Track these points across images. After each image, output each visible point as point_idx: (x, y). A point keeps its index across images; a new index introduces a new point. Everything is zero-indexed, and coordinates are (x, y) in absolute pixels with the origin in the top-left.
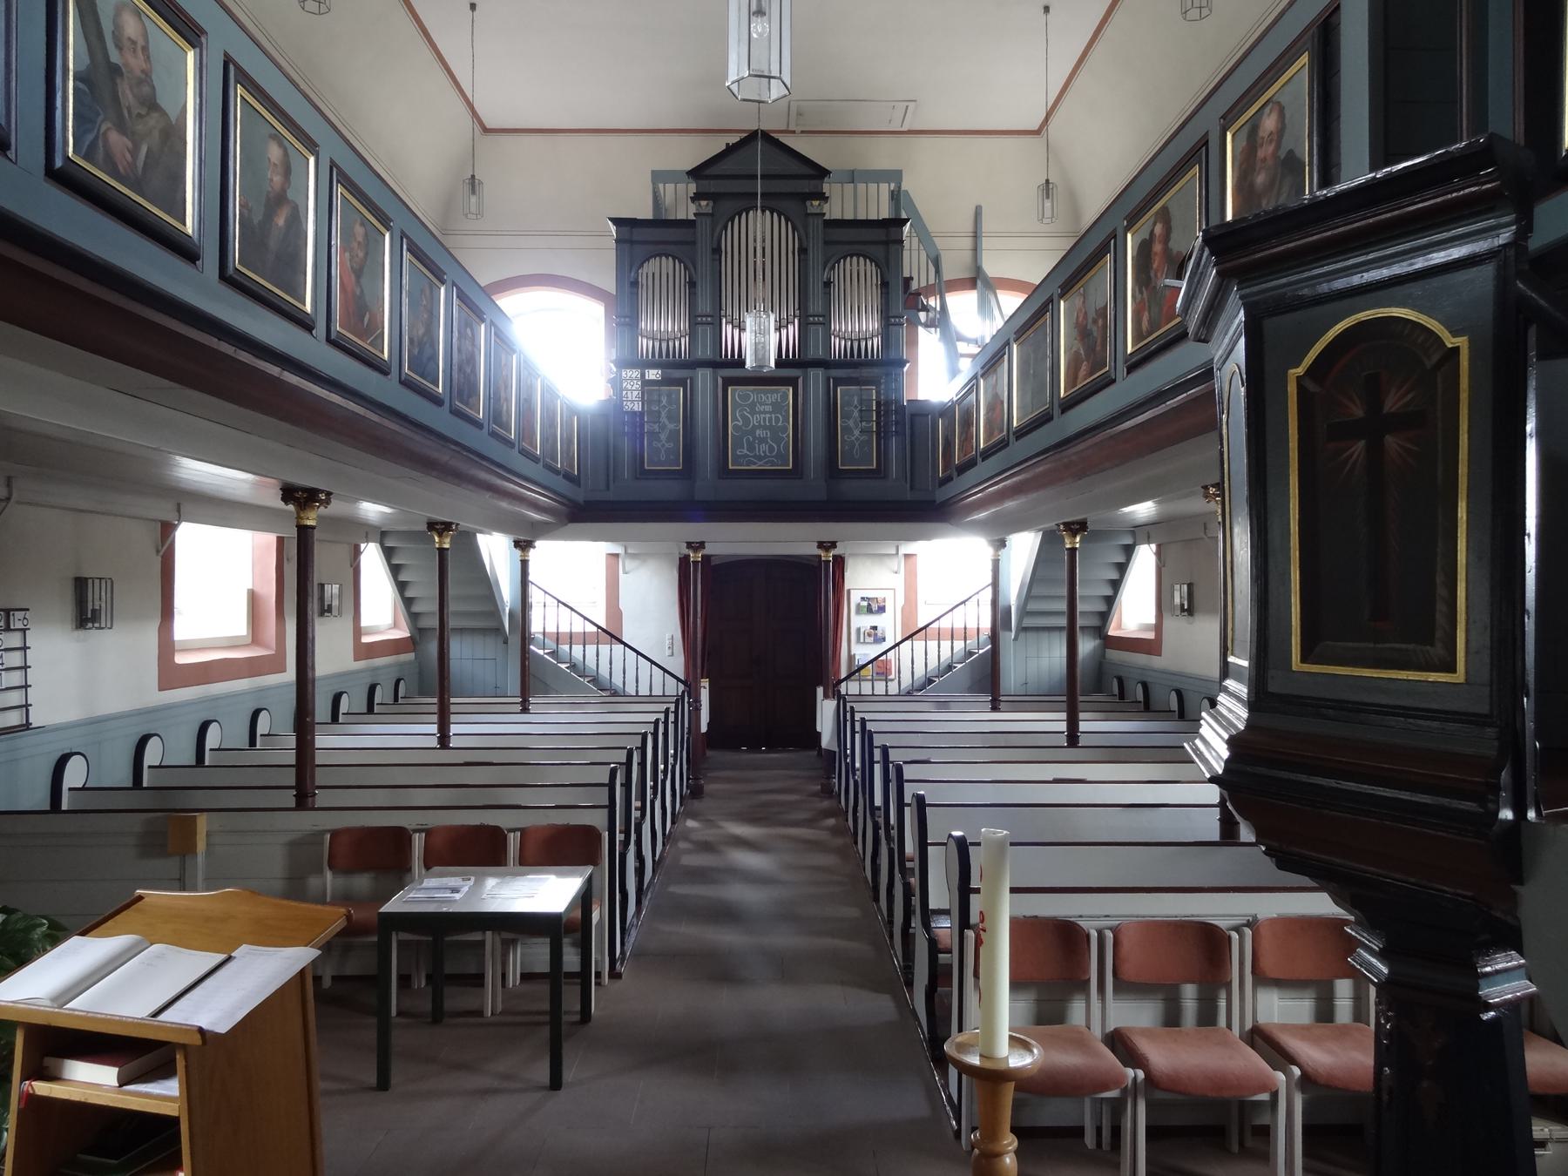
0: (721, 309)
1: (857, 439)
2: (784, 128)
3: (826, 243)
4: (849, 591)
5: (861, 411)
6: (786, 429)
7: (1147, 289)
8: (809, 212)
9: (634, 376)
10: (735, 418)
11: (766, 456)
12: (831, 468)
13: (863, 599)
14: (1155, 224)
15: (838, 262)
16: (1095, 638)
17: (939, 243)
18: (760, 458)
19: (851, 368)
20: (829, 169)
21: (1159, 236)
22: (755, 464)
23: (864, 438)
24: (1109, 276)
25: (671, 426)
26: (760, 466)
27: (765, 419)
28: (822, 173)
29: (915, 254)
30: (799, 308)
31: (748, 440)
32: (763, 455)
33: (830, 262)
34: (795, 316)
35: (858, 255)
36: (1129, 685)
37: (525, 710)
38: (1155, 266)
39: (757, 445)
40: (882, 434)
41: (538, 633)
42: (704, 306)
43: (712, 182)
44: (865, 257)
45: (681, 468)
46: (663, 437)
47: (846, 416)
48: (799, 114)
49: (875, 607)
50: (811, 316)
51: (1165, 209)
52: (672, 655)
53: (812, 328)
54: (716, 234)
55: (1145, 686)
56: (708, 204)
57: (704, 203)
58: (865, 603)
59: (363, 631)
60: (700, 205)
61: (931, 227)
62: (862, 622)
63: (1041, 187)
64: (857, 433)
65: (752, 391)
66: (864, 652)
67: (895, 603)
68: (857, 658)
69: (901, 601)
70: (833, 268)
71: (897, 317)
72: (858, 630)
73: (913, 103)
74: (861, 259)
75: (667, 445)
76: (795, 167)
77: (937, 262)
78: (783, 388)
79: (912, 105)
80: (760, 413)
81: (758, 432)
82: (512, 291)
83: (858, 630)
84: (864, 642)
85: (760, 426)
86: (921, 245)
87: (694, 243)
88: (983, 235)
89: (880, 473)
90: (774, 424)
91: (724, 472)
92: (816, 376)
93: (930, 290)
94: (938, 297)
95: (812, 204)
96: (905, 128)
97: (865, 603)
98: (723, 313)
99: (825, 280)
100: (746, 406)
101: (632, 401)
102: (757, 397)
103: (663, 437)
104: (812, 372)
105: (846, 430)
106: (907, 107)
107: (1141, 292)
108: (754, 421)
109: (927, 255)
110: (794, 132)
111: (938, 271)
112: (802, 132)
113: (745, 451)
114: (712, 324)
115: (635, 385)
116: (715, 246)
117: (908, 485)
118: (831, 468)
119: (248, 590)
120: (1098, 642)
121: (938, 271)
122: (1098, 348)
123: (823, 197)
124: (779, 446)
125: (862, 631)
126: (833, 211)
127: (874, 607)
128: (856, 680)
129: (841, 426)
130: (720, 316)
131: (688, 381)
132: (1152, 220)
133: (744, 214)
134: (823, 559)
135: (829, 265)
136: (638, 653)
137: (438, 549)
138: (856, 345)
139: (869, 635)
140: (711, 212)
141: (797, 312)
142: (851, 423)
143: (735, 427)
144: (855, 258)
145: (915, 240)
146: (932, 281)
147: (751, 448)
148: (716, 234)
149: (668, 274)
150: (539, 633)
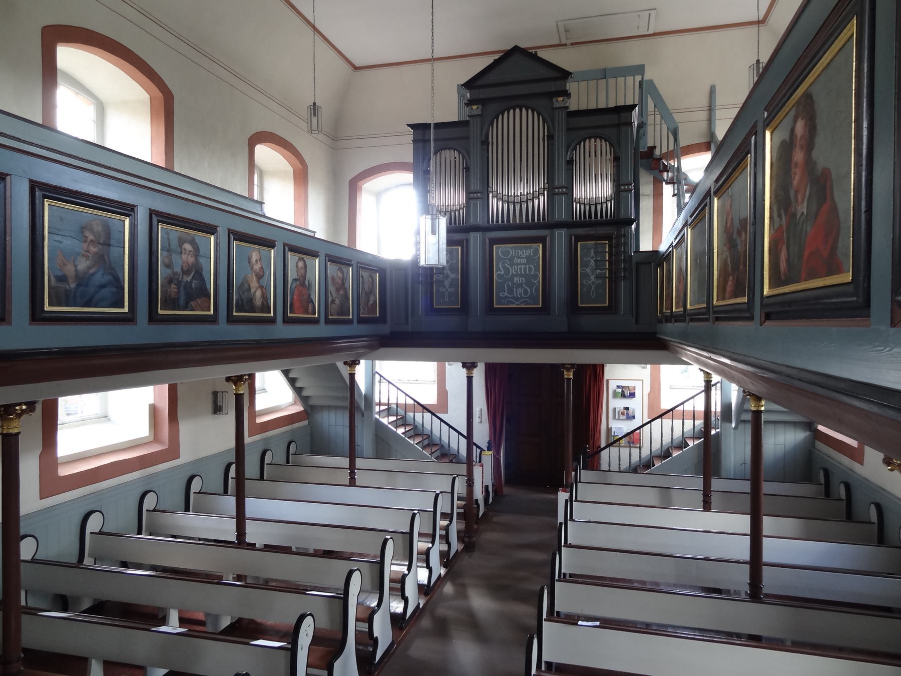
0: (488, 186)
1: (593, 283)
2: (557, 42)
3: (569, 129)
4: (608, 381)
5: (596, 261)
6: (536, 276)
7: (786, 214)
8: (555, 106)
10: (498, 269)
11: (522, 297)
12: (572, 306)
13: (618, 387)
14: (795, 121)
15: (579, 144)
16: (805, 430)
17: (677, 117)
18: (517, 299)
19: (589, 227)
20: (571, 71)
21: (801, 138)
22: (513, 303)
23: (599, 281)
24: (749, 181)
25: (452, 276)
26: (518, 305)
27: (521, 269)
28: (565, 75)
29: (658, 127)
30: (548, 183)
31: (509, 284)
32: (519, 296)
33: (572, 146)
34: (544, 189)
35: (595, 137)
36: (835, 480)
37: (352, 483)
38: (795, 182)
39: (515, 289)
40: (614, 279)
41: (393, 404)
42: (476, 185)
43: (481, 90)
44: (601, 138)
45: (459, 307)
46: (447, 283)
47: (585, 265)
48: (566, 31)
49: (627, 393)
50: (557, 188)
51: (808, 96)
52: (481, 422)
53: (557, 197)
54: (484, 130)
55: (848, 487)
56: (478, 108)
57: (475, 107)
58: (620, 390)
59: (257, 414)
60: (472, 109)
61: (670, 105)
62: (619, 404)
63: (752, 67)
64: (592, 278)
65: (512, 248)
66: (621, 427)
67: (643, 391)
68: (613, 430)
69: (647, 390)
70: (575, 149)
71: (626, 185)
72: (615, 409)
73: (655, 11)
74: (598, 140)
75: (449, 290)
76: (544, 72)
77: (675, 133)
78: (535, 245)
79: (653, 13)
80: (517, 264)
81: (515, 279)
82: (375, 176)
83: (615, 409)
84: (619, 419)
85: (517, 275)
86: (663, 121)
87: (467, 138)
88: (717, 108)
89: (612, 308)
90: (528, 272)
91: (490, 308)
92: (561, 235)
93: (670, 155)
94: (676, 160)
95: (557, 101)
96: (651, 32)
97: (620, 390)
98: (490, 189)
99: (568, 159)
100: (507, 259)
102: (515, 252)
103: (447, 283)
104: (557, 232)
105: (585, 276)
106: (650, 14)
107: (780, 216)
108: (513, 271)
109: (668, 127)
110: (565, 45)
111: (676, 140)
112: (572, 44)
113: (506, 294)
114: (481, 198)
116: (483, 138)
117: (634, 320)
118: (572, 306)
119: (150, 405)
120: (808, 433)
121: (676, 140)
122: (741, 267)
123: (566, 94)
124: (531, 290)
125: (617, 410)
126: (573, 104)
127: (627, 393)
128: (617, 446)
129: (580, 272)
130: (488, 192)
131: (465, 241)
132: (793, 113)
133: (506, 113)
134: (565, 376)
135: (571, 147)
136: (450, 426)
137: (235, 394)
138: (593, 208)
139: (623, 414)
140: (480, 113)
141: (546, 186)
142: (588, 270)
143: (499, 276)
144: (593, 140)
145: (658, 117)
146: (671, 148)
147: (511, 291)
148: (484, 130)
149: (450, 162)
150: (394, 404)
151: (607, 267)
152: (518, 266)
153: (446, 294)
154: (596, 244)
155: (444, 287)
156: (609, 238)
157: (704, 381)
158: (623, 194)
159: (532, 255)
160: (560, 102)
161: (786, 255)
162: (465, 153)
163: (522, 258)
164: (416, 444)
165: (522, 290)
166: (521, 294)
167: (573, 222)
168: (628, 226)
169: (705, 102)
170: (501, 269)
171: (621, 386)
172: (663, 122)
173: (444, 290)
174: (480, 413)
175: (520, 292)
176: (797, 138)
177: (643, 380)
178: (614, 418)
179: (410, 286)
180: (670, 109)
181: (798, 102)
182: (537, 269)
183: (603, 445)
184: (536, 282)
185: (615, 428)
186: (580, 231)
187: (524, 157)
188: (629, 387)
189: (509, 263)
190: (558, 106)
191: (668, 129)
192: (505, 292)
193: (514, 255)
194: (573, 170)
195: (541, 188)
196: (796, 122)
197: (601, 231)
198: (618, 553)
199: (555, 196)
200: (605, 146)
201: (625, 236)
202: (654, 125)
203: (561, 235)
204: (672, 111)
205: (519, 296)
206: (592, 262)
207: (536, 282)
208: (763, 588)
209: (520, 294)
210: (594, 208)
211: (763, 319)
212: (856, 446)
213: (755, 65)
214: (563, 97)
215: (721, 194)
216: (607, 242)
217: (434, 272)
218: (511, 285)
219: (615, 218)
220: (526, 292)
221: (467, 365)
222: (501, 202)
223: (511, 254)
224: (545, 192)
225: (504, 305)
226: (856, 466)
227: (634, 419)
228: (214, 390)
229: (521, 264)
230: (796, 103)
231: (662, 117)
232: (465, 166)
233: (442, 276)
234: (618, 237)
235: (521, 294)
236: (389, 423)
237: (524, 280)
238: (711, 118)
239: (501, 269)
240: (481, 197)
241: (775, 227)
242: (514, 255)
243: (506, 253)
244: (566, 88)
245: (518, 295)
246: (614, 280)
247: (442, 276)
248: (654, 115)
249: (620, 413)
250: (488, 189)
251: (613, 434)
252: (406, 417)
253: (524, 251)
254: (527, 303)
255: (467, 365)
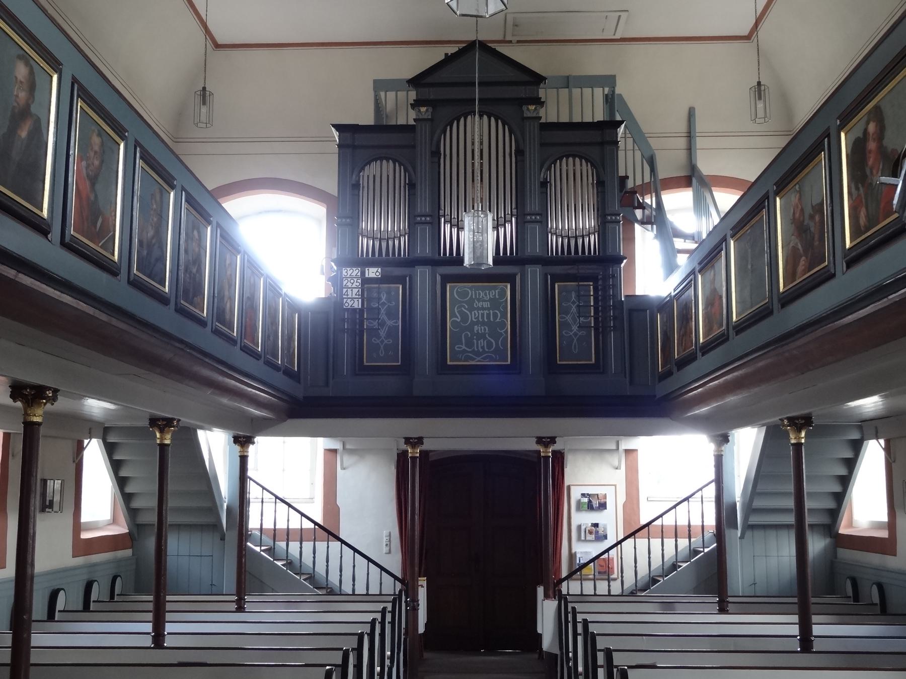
0: (439, 209)
1: (575, 334)
3: (542, 145)
4: (569, 488)
5: (578, 306)
6: (503, 325)
7: (863, 186)
8: (525, 115)
9: (354, 274)
10: (453, 315)
13: (583, 495)
14: (868, 123)
17: (653, 142)
18: (478, 354)
20: (543, 75)
21: (873, 134)
22: (473, 359)
25: (390, 323)
27: (483, 315)
28: (537, 79)
29: (630, 154)
30: (517, 208)
31: (466, 335)
32: (481, 350)
33: (547, 163)
39: (475, 341)
40: (601, 329)
42: (424, 206)
43: (431, 89)
44: (581, 158)
46: (383, 333)
47: (565, 311)
49: (595, 503)
51: (877, 108)
52: (390, 552)
53: (529, 226)
54: (435, 139)
56: (427, 110)
57: (423, 109)
58: (586, 500)
59: (82, 526)
61: (645, 128)
62: (582, 519)
64: (575, 328)
65: (471, 288)
66: (586, 550)
67: (616, 500)
68: (578, 556)
70: (549, 169)
72: (579, 527)
75: (386, 342)
77: (652, 162)
78: (501, 285)
80: (478, 309)
81: (476, 328)
83: (579, 527)
84: (586, 540)
85: (477, 323)
87: (414, 147)
89: (599, 368)
90: (492, 320)
91: (442, 366)
92: (534, 274)
93: (645, 189)
94: (654, 194)
95: (528, 109)
96: (618, 36)
98: (442, 212)
101: (352, 299)
103: (383, 333)
104: (529, 269)
105: (565, 325)
107: (857, 189)
108: (472, 316)
110: (510, 42)
111: (653, 170)
112: (518, 42)
113: (464, 347)
115: (355, 284)
116: (434, 149)
121: (653, 170)
122: (816, 243)
123: (539, 102)
124: (497, 344)
125: (583, 528)
127: (595, 504)
131: (408, 278)
132: (865, 118)
135: (546, 166)
136: (355, 550)
139: (591, 533)
140: (430, 117)
141: (515, 211)
142: (569, 318)
143: (454, 323)
144: (571, 159)
147: (469, 343)
148: (435, 139)
151: (592, 314)
152: (479, 311)
153: (382, 346)
154: (579, 286)
155: (379, 337)
156: (594, 278)
157: (714, 455)
158: (610, 226)
159: (497, 297)
160: (532, 112)
161: (865, 213)
162: (409, 164)
163: (485, 301)
164: (305, 580)
165: (485, 342)
166: (483, 347)
167: (549, 257)
168: (616, 265)
169: (682, 127)
170: (457, 314)
171: (588, 494)
172: (636, 148)
173: (378, 341)
174: (388, 538)
175: (482, 345)
176: (869, 135)
177: (615, 486)
178: (579, 539)
179: (331, 336)
180: (644, 131)
181: (870, 112)
182: (504, 315)
183: (564, 573)
184: (502, 331)
185: (581, 553)
186: (559, 270)
187: (486, 175)
188: (598, 495)
189: (467, 307)
190: (529, 115)
191: (643, 156)
192: (462, 344)
193: (474, 297)
194: (547, 194)
195: (508, 214)
196: (869, 124)
197: (584, 269)
198: (644, 637)
199: (526, 224)
200: (586, 168)
201: (613, 276)
202: (633, 150)
203: (534, 274)
204: (646, 135)
205: (481, 350)
206: (574, 309)
207: (502, 331)
208: (814, 642)
209: (481, 347)
210: (574, 241)
211: (845, 269)
212: (887, 536)
213: (756, 87)
214: (536, 105)
215: (784, 193)
216: (591, 283)
217: (365, 317)
218: (469, 336)
219: (601, 254)
220: (489, 345)
221: (411, 440)
222: (456, 229)
223: (470, 296)
224: (513, 219)
225: (459, 361)
226: (890, 562)
227: (606, 538)
228: (42, 478)
229: (483, 309)
230: (867, 113)
231: (634, 141)
232: (407, 182)
233: (376, 323)
234: (605, 278)
235: (483, 347)
236: (261, 550)
237: (487, 329)
238: (690, 146)
239: (457, 314)
240: (431, 221)
241: (854, 198)
242: (474, 297)
243: (464, 294)
244: (538, 95)
245: (480, 348)
246: (601, 330)
247: (376, 323)
248: (625, 137)
249: (587, 531)
250: (439, 212)
251: (578, 562)
252: (274, 548)
253: (487, 292)
254: (491, 359)
255: (411, 440)
